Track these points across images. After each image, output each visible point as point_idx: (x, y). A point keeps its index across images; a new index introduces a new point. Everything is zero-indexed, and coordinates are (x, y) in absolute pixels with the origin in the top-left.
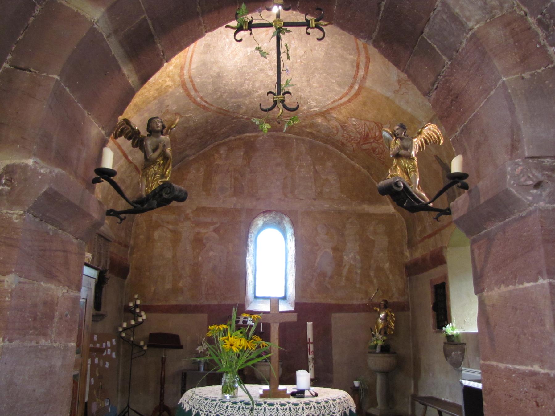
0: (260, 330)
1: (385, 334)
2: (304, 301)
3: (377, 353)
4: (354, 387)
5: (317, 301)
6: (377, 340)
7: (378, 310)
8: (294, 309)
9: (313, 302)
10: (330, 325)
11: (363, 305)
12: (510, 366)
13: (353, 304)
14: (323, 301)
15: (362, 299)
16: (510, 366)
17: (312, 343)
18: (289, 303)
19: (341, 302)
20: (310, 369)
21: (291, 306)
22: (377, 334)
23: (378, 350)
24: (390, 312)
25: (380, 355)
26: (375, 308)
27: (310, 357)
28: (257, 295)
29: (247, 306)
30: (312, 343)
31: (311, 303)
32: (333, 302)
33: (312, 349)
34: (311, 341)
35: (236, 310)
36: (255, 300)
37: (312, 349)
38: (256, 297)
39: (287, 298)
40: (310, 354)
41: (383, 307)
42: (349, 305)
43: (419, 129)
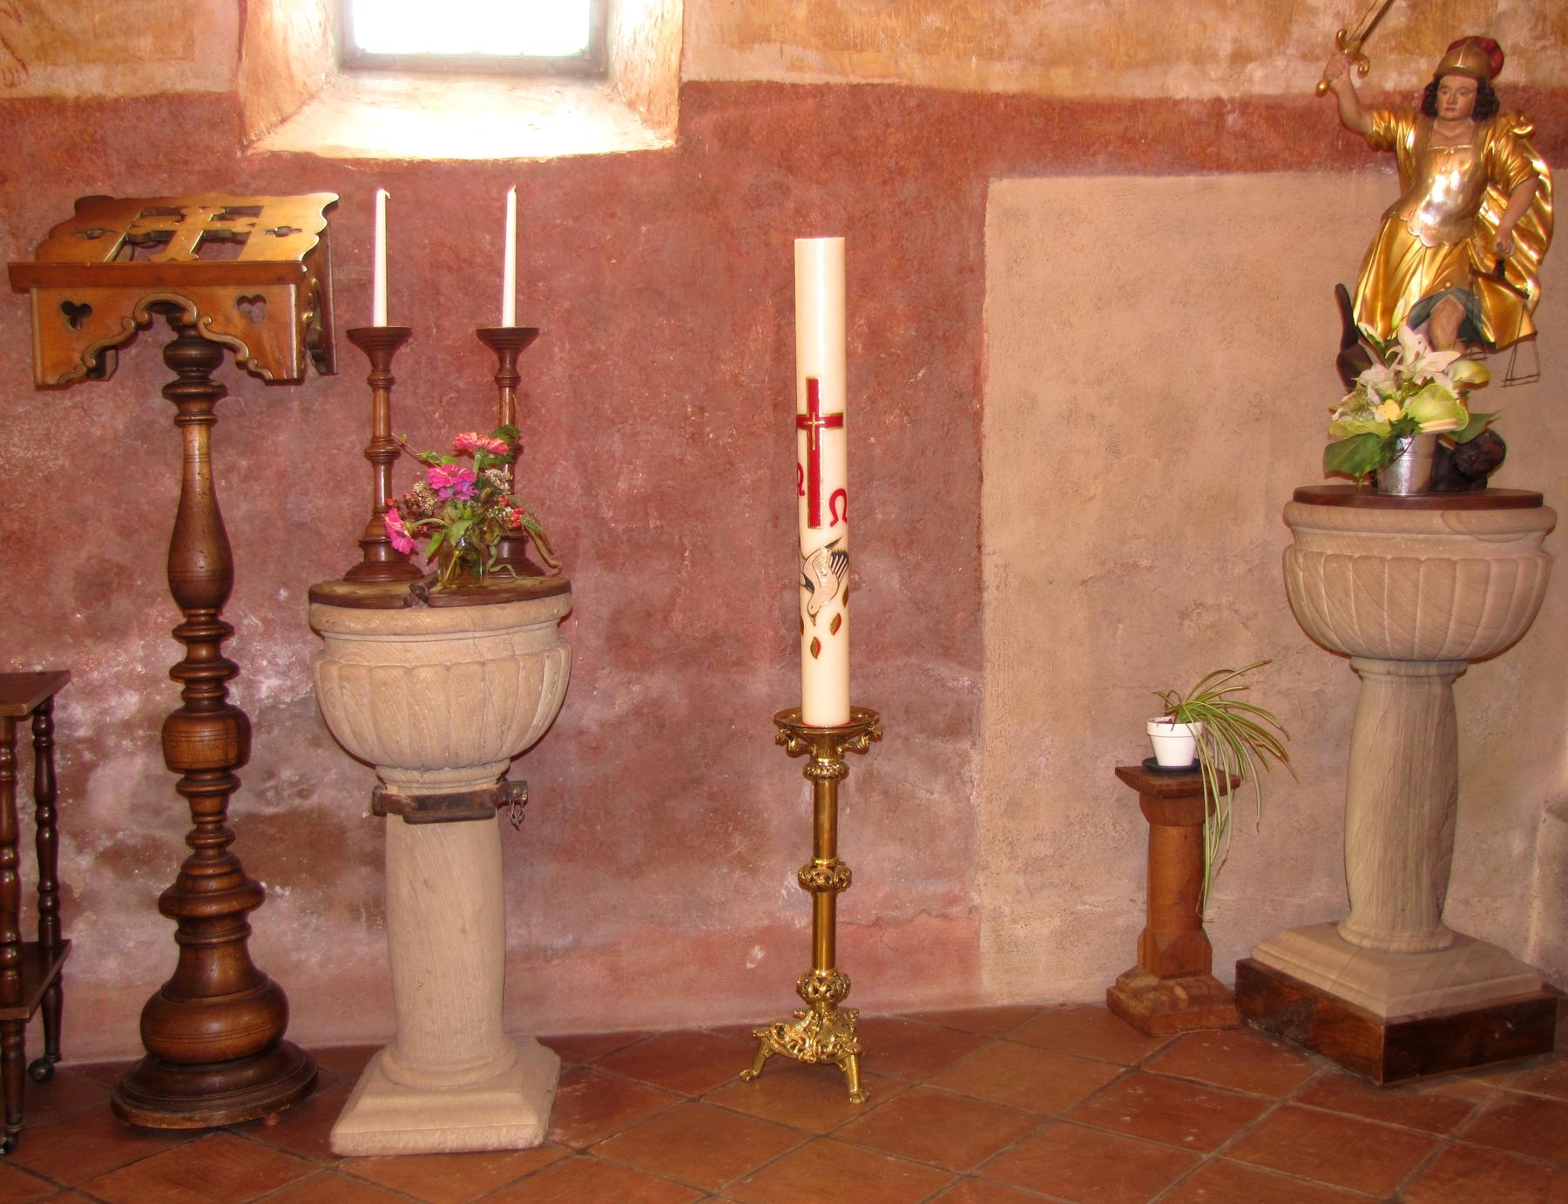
0: (370, 317)
1: (1469, 337)
2: (764, 75)
3: (1398, 503)
4: (1152, 765)
5: (863, 69)
6: (1410, 387)
7: (1408, 136)
8: (670, 143)
9: (835, 79)
10: (974, 270)
11: (1245, 106)
12: (196, 444)
13: (1166, 104)
14: (916, 71)
15: (1241, 57)
16: (196, 444)
17: (835, 421)
18: (631, 105)
19: (1065, 84)
20: (816, 647)
21: (650, 122)
22: (1411, 341)
23: (1407, 471)
24: (1518, 143)
25: (1435, 519)
26: (1376, 125)
27: (819, 539)
28: (368, 41)
29: (259, 121)
30: (835, 421)
31: (820, 91)
32: (1004, 79)
33: (832, 475)
34: (831, 401)
35: (836, 731)
36: (345, 80)
37: (832, 475)
38: (352, 63)
39: (617, 66)
40: (814, 521)
41: (1462, 102)
42: (1136, 108)
43: (267, 883)
